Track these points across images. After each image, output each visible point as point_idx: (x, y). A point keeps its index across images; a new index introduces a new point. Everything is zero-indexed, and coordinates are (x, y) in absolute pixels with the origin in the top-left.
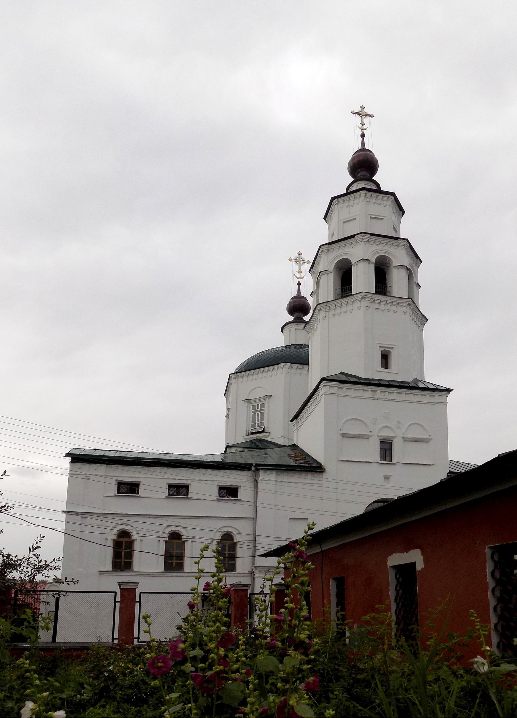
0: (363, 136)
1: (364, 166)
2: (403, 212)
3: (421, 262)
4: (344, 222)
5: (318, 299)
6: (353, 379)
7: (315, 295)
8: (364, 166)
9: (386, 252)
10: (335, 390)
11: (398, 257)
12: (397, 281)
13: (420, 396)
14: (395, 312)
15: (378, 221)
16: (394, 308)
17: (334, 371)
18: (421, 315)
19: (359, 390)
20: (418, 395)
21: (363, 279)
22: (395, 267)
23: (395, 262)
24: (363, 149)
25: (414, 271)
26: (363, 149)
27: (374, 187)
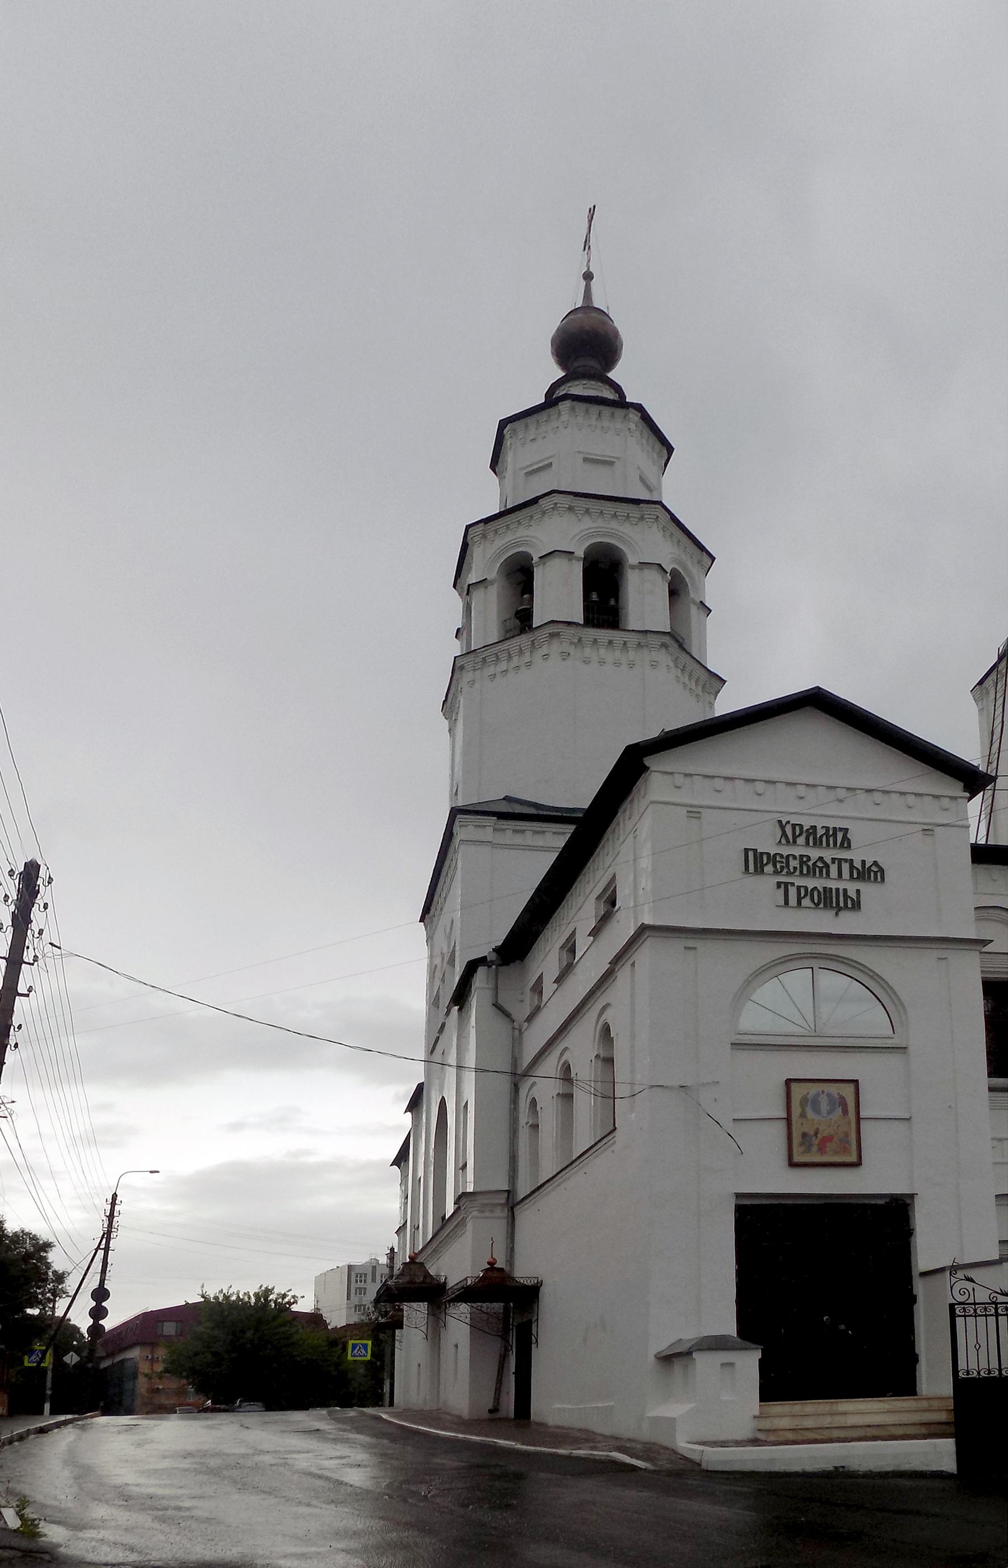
0: (588, 276)
1: (587, 347)
2: (670, 450)
3: (713, 559)
4: (530, 474)
5: (469, 643)
6: (519, 809)
7: (465, 634)
8: (587, 347)
9: (611, 535)
10: (488, 834)
11: (642, 545)
12: (644, 601)
13: (509, 833)
14: (617, 664)
15: (603, 470)
16: (609, 656)
17: (492, 793)
18: (706, 674)
19: (544, 832)
20: (544, 832)
21: (559, 593)
22: (633, 567)
23: (632, 559)
24: (588, 307)
25: (692, 578)
26: (588, 307)
27: (609, 394)
